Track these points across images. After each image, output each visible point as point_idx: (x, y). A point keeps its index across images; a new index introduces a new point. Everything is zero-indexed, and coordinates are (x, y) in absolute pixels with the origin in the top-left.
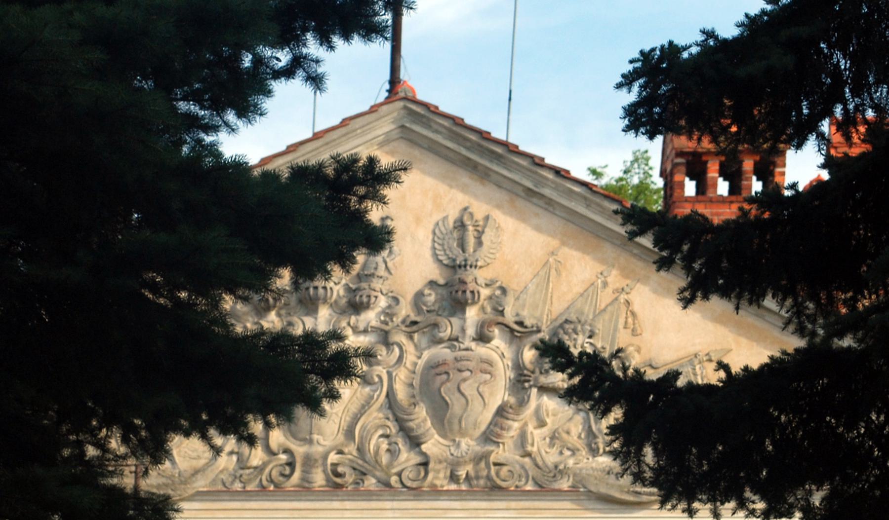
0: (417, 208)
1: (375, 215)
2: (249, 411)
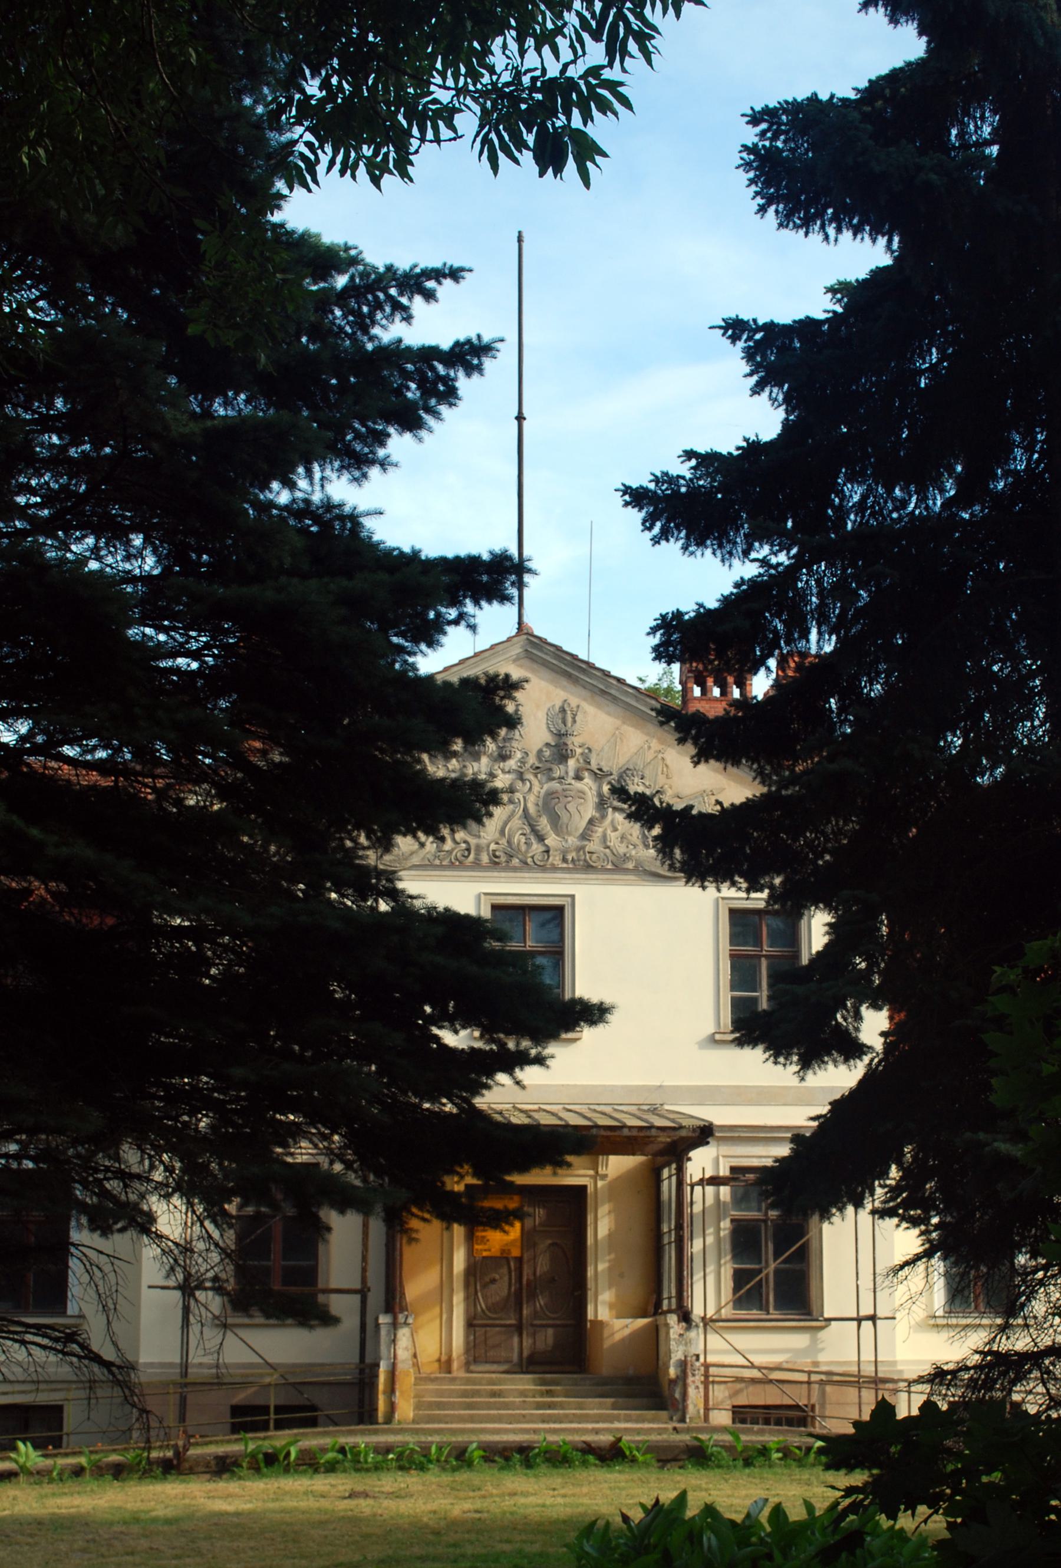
0: (537, 702)
1: (510, 708)
2: (441, 822)
